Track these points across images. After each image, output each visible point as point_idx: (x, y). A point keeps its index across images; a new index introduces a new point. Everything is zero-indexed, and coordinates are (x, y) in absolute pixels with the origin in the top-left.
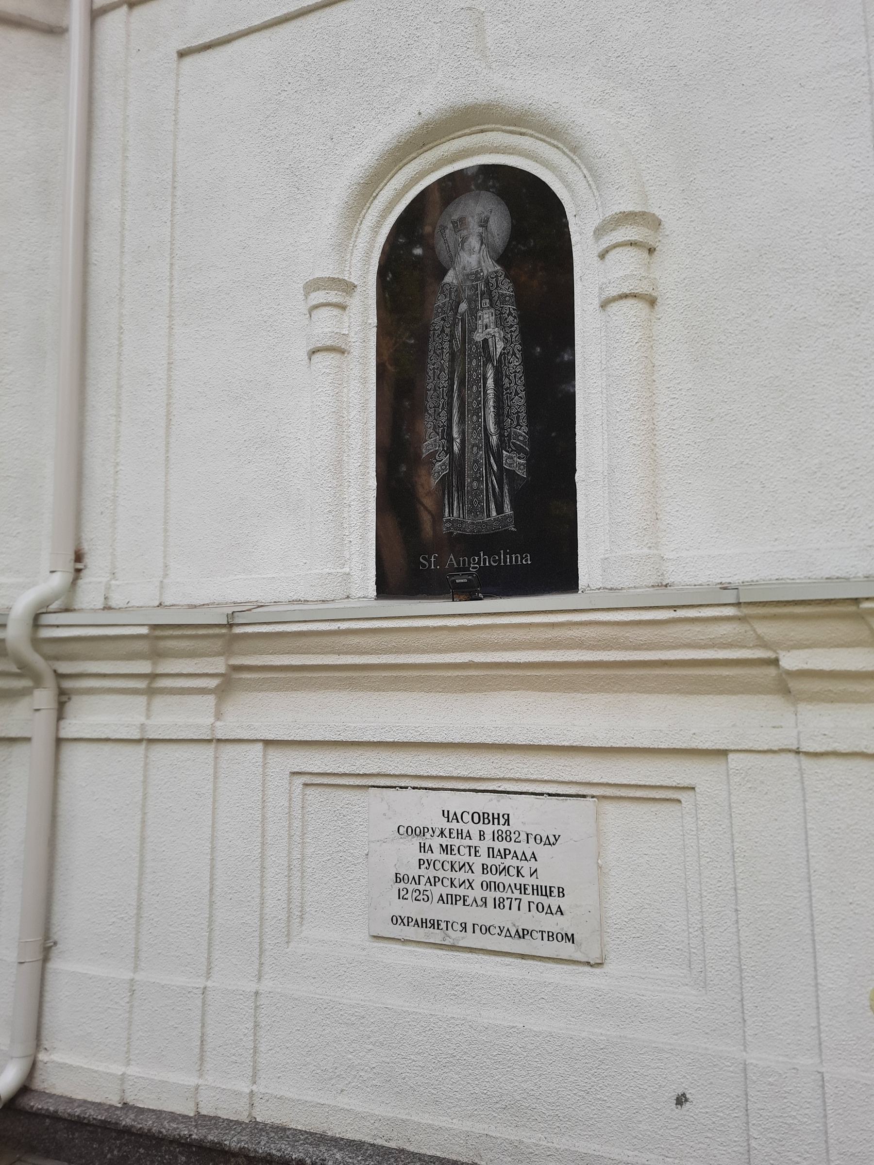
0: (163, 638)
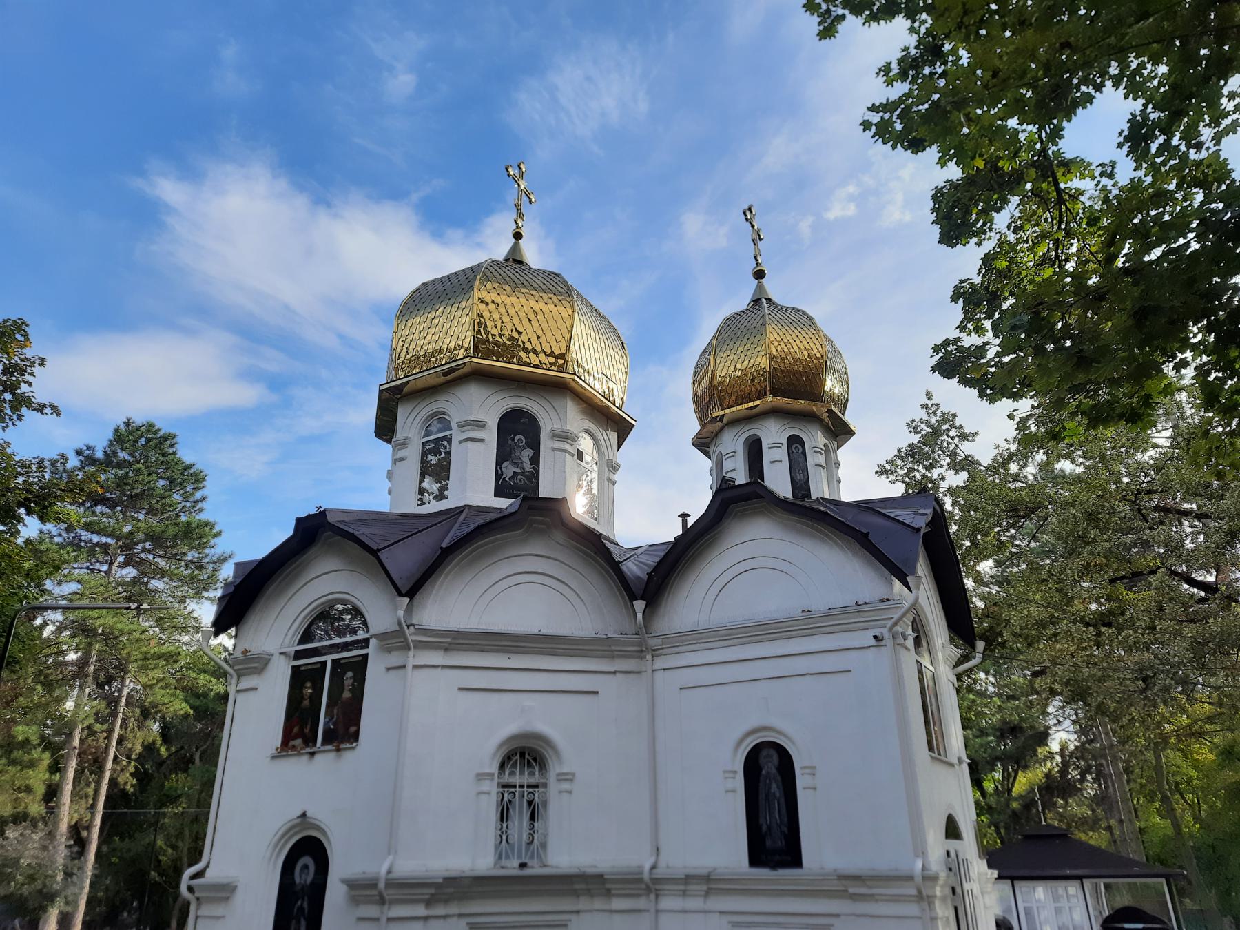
0: (689, 879)
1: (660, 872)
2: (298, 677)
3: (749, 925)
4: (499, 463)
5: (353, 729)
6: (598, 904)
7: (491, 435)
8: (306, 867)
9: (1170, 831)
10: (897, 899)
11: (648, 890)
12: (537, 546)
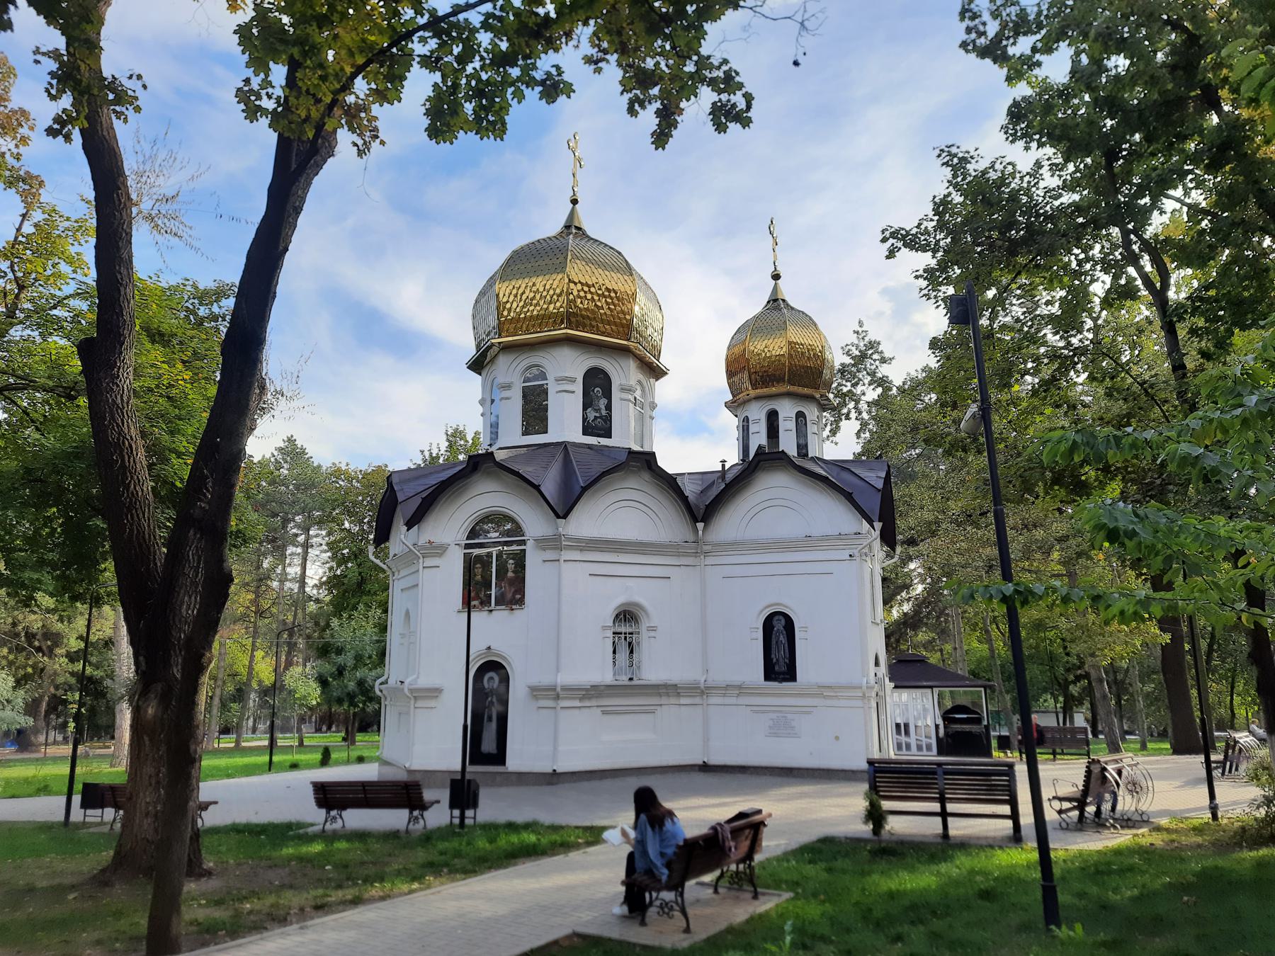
0: (728, 687)
1: (710, 683)
2: (469, 564)
3: (763, 712)
4: (585, 409)
5: (518, 596)
6: (673, 700)
7: (578, 388)
8: (491, 678)
9: (986, 653)
10: (850, 698)
11: (702, 693)
12: (632, 482)
